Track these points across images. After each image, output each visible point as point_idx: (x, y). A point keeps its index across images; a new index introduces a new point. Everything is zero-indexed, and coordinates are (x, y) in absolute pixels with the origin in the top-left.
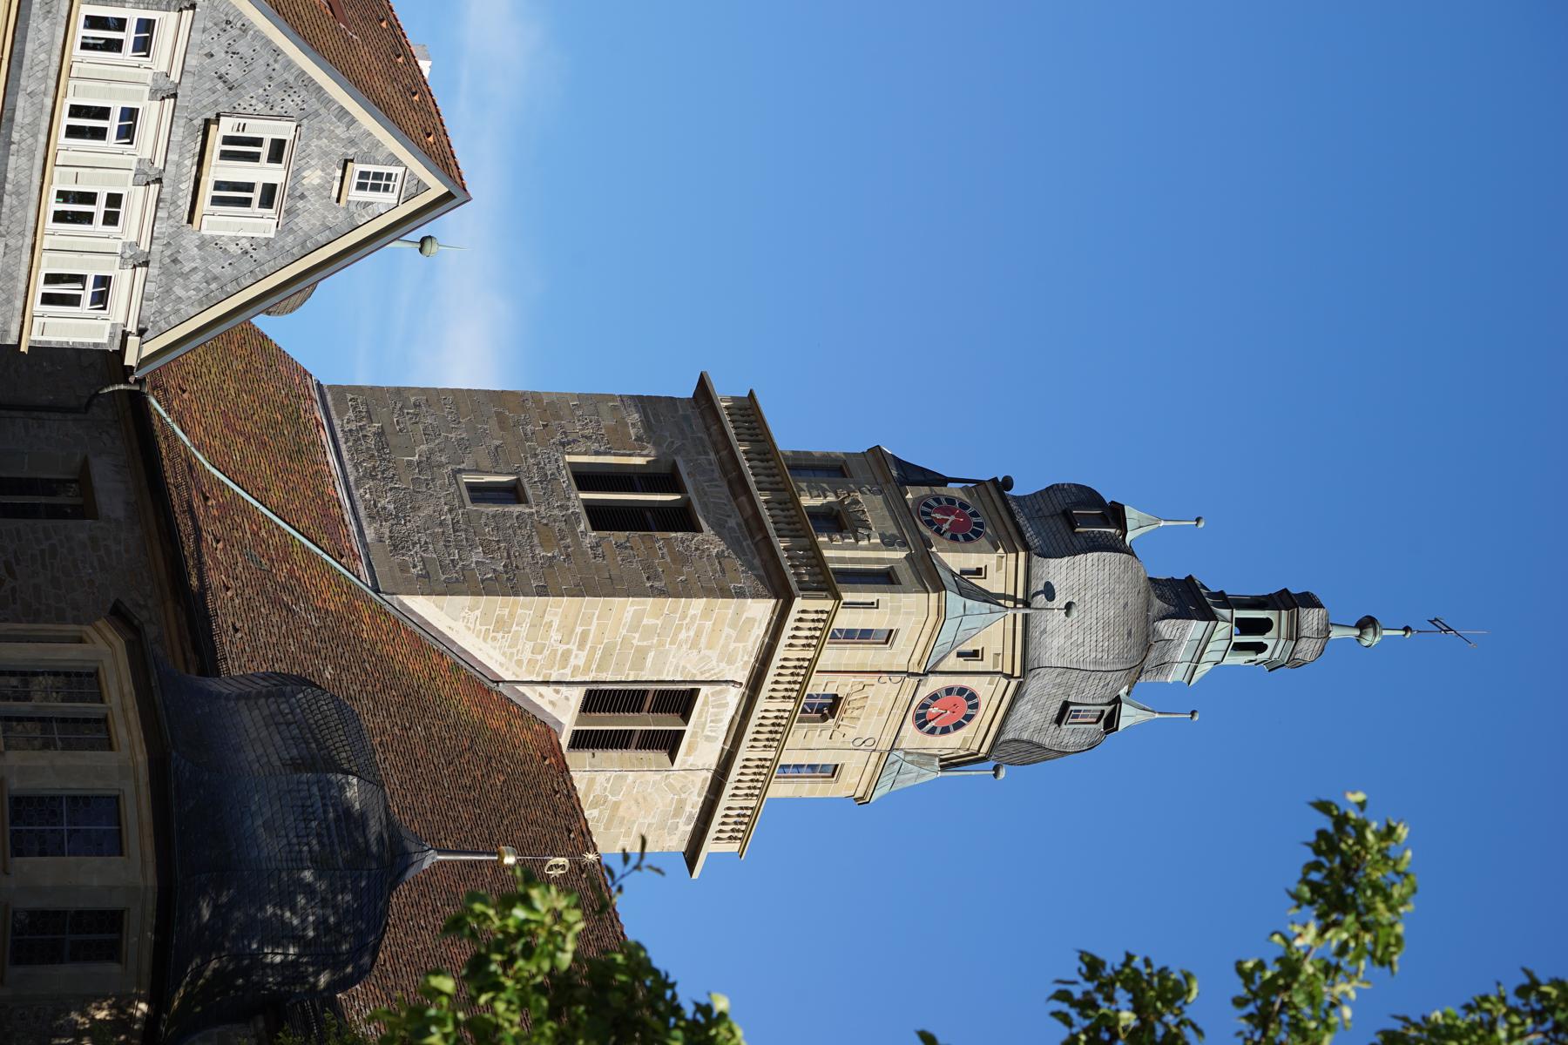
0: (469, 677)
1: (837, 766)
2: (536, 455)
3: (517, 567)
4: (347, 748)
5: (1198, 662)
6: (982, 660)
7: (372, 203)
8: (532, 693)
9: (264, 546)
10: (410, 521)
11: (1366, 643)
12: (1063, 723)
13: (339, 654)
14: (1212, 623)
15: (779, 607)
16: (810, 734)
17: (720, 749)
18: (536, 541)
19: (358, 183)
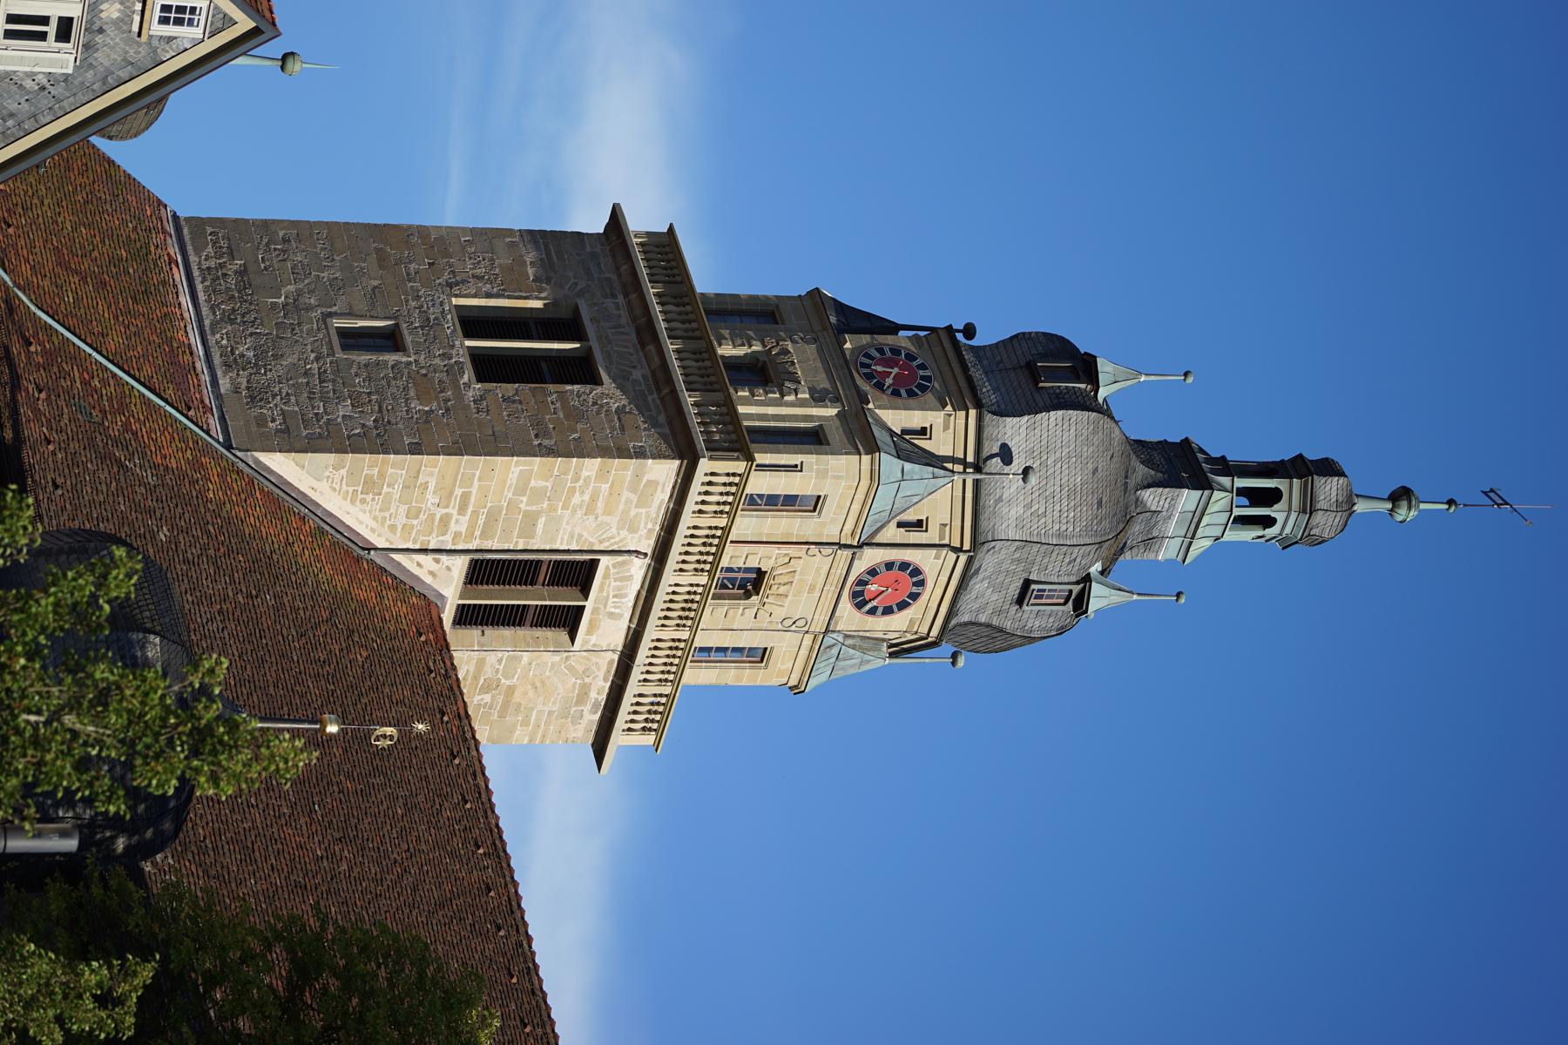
0: (335, 544)
1: (766, 649)
2: (418, 297)
3: (389, 422)
4: (151, 607)
5: (1193, 538)
6: (926, 531)
7: (175, 38)
8: (408, 561)
9: (96, 397)
10: (271, 370)
11: (1400, 518)
12: (1025, 605)
13: (178, 514)
14: (1207, 493)
15: (683, 468)
16: (731, 612)
17: (626, 627)
18: (412, 393)
19: (160, 17)
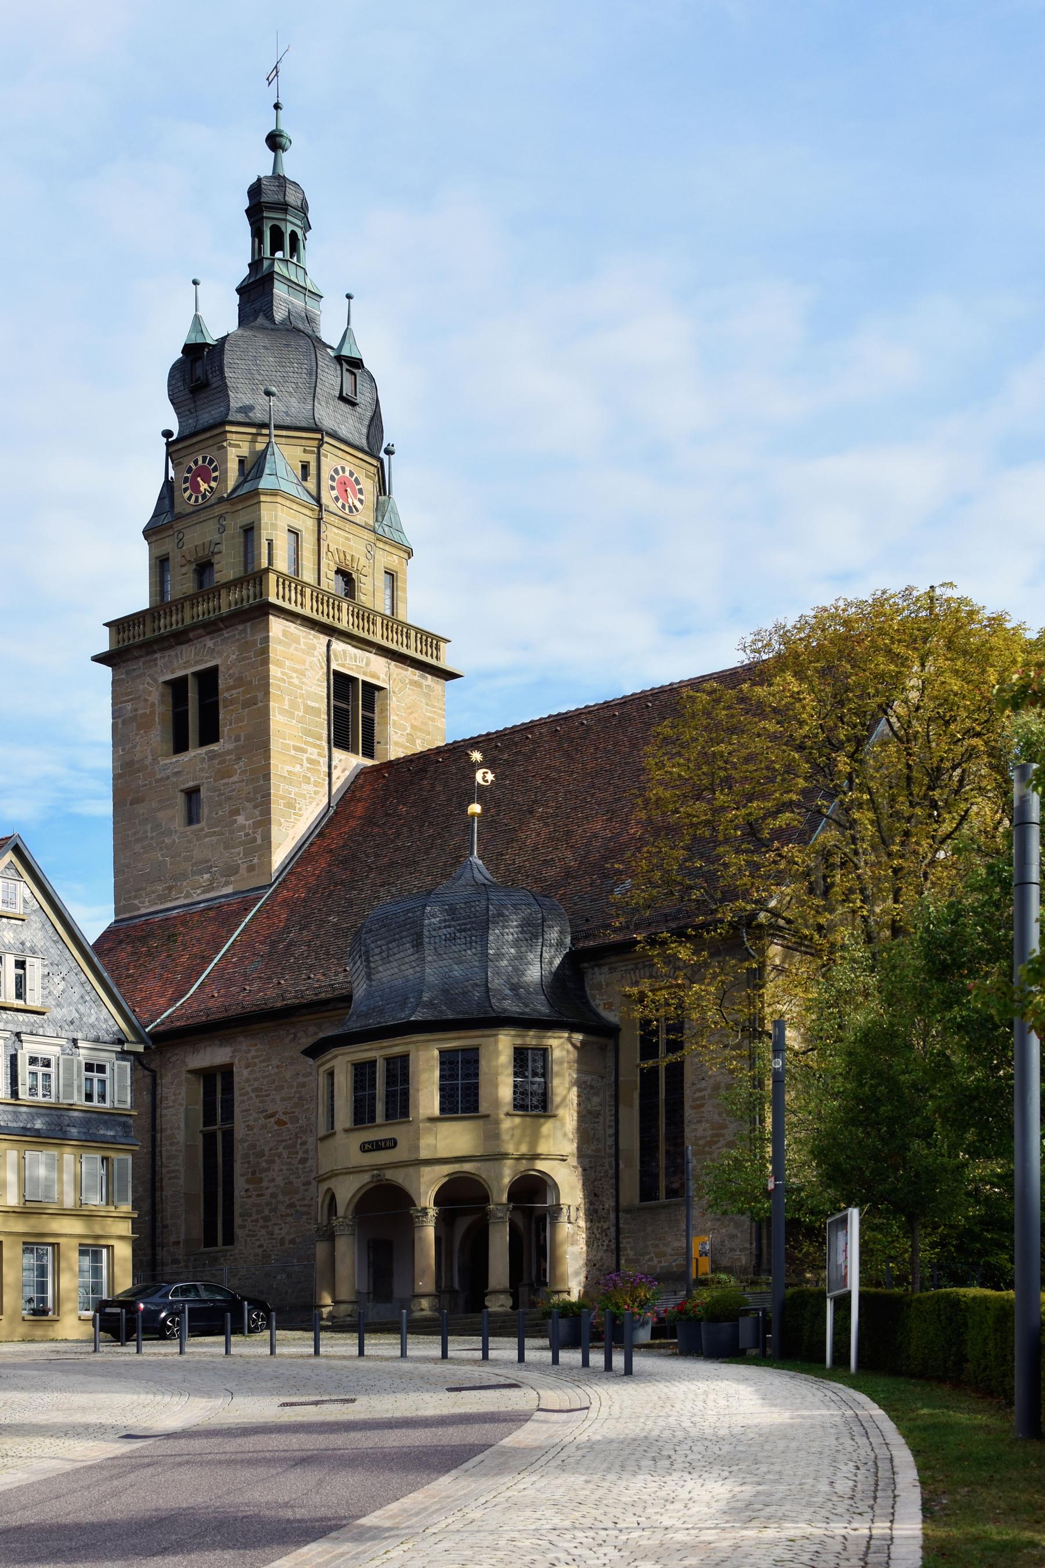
14: (275, 276)
